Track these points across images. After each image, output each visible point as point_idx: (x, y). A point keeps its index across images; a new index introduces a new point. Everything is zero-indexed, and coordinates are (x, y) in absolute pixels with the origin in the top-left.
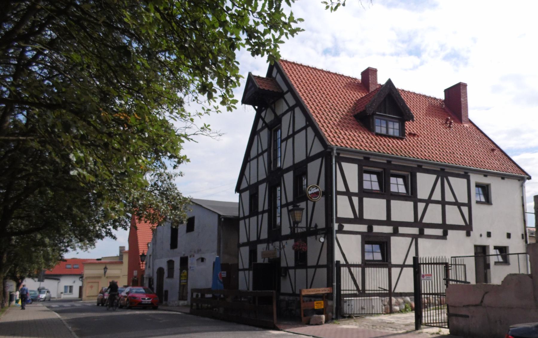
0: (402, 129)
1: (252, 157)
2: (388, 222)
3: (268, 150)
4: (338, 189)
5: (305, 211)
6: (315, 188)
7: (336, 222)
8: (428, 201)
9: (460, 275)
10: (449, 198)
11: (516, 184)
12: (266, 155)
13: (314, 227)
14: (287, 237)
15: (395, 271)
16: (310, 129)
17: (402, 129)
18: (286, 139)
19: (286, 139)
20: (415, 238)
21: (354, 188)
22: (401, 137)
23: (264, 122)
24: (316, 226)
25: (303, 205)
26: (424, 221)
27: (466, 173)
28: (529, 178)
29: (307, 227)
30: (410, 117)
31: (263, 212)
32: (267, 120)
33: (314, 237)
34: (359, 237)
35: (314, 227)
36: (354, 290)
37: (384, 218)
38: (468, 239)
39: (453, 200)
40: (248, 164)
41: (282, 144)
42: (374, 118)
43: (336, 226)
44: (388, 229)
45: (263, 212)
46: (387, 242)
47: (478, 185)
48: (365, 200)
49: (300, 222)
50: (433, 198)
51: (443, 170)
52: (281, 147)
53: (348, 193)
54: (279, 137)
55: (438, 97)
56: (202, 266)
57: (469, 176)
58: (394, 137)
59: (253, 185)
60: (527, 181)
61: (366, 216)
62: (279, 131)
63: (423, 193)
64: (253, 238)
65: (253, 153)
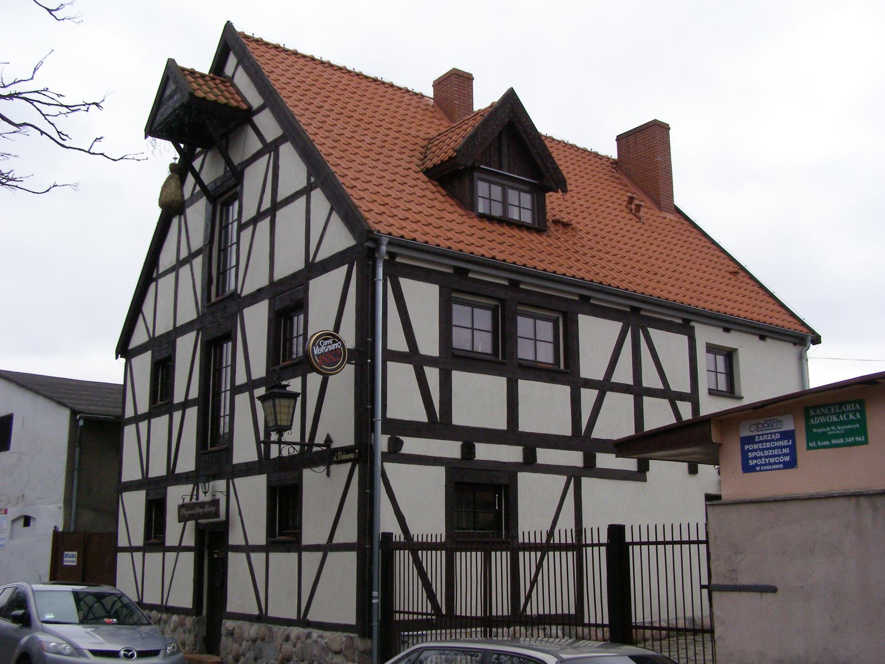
0: (539, 208)
1: (162, 269)
3: (206, 250)
4: (391, 346)
5: (299, 399)
6: (330, 341)
7: (384, 432)
8: (605, 386)
10: (650, 379)
11: (788, 351)
12: (198, 262)
13: (322, 442)
15: (527, 561)
16: (318, 195)
17: (539, 208)
18: (254, 221)
19: (254, 221)
20: (574, 475)
21: (429, 345)
22: (536, 226)
23: (199, 181)
24: (329, 440)
25: (294, 385)
26: (596, 434)
27: (685, 320)
28: (817, 340)
29: (302, 444)
30: (559, 184)
31: (185, 405)
32: (207, 178)
33: (322, 468)
34: (441, 471)
35: (322, 442)
37: (502, 424)
38: (693, 480)
39: (660, 386)
40: (153, 286)
41: (242, 234)
42: (475, 178)
43: (382, 442)
44: (512, 454)
45: (185, 405)
46: (506, 487)
47: (712, 349)
48: (457, 376)
49: (289, 428)
50: (615, 379)
52: (238, 243)
54: (236, 217)
55: (602, 152)
56: (25, 536)
57: (693, 328)
58: (519, 225)
59: (161, 336)
60: (812, 348)
61: (459, 419)
62: (237, 204)
64: (158, 469)
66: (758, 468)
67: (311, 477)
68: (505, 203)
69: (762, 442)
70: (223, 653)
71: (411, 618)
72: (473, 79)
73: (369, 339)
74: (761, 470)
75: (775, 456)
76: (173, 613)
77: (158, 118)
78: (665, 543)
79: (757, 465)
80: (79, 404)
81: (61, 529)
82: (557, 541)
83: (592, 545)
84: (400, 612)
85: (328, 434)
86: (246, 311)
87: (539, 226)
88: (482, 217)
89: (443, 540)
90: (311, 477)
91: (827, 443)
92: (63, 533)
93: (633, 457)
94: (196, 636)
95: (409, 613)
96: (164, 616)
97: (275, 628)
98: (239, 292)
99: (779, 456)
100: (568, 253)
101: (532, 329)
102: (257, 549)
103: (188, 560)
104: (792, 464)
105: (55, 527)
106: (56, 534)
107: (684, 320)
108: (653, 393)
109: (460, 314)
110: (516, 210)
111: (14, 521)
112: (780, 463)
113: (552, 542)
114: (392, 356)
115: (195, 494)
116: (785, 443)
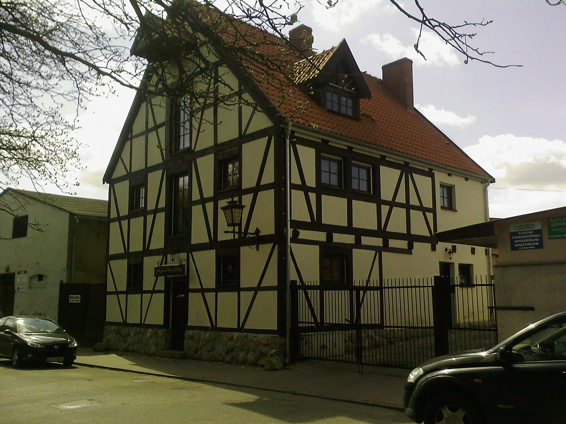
0: (356, 107)
2: (349, 229)
8: (392, 204)
9: (340, 302)
10: (414, 201)
14: (201, 247)
20: (378, 250)
21: (311, 182)
24: (258, 231)
32: (170, 81)
34: (317, 248)
36: (311, 323)
37: (345, 224)
38: (433, 254)
40: (128, 143)
43: (290, 232)
44: (349, 239)
47: (442, 186)
48: (324, 197)
51: (407, 164)
53: (303, 187)
58: (348, 117)
63: (386, 194)
64: (136, 246)
65: (139, 127)
66: (520, 248)
67: (246, 252)
68: (340, 104)
69: (523, 235)
70: (186, 349)
71: (304, 325)
72: (312, 31)
73: (283, 178)
74: (521, 249)
75: (530, 242)
76: (150, 328)
77: (139, 45)
78: (403, 287)
79: (519, 246)
80: (64, 206)
81: (65, 282)
82: (372, 285)
83: (388, 288)
84: (303, 322)
85: (257, 228)
86: (198, 160)
87: (356, 117)
88: (329, 111)
89: (318, 284)
90: (246, 252)
91: (560, 236)
92: (67, 285)
93: (451, 241)
94: (166, 340)
95: (305, 323)
96: (142, 330)
97: (223, 333)
98: (193, 149)
99: (532, 242)
100: (312, 119)
101: (358, 174)
102: (122, 293)
103: (160, 299)
104: (540, 246)
105: (61, 281)
106: (62, 285)
107: (429, 169)
108: (415, 208)
109: (325, 165)
110: (109, 48)
111: (31, 278)
112: (533, 246)
113: (369, 285)
114: (294, 186)
115: (164, 260)
116: (536, 236)
